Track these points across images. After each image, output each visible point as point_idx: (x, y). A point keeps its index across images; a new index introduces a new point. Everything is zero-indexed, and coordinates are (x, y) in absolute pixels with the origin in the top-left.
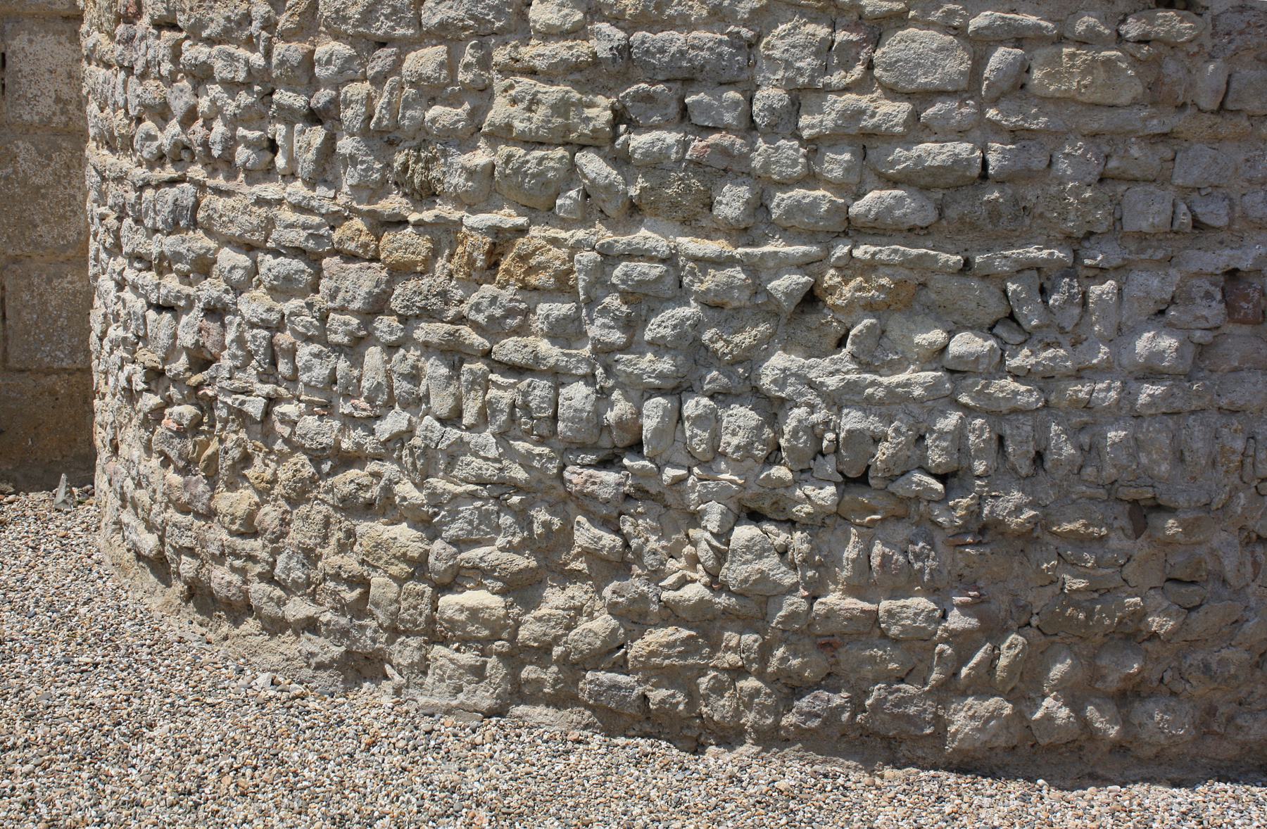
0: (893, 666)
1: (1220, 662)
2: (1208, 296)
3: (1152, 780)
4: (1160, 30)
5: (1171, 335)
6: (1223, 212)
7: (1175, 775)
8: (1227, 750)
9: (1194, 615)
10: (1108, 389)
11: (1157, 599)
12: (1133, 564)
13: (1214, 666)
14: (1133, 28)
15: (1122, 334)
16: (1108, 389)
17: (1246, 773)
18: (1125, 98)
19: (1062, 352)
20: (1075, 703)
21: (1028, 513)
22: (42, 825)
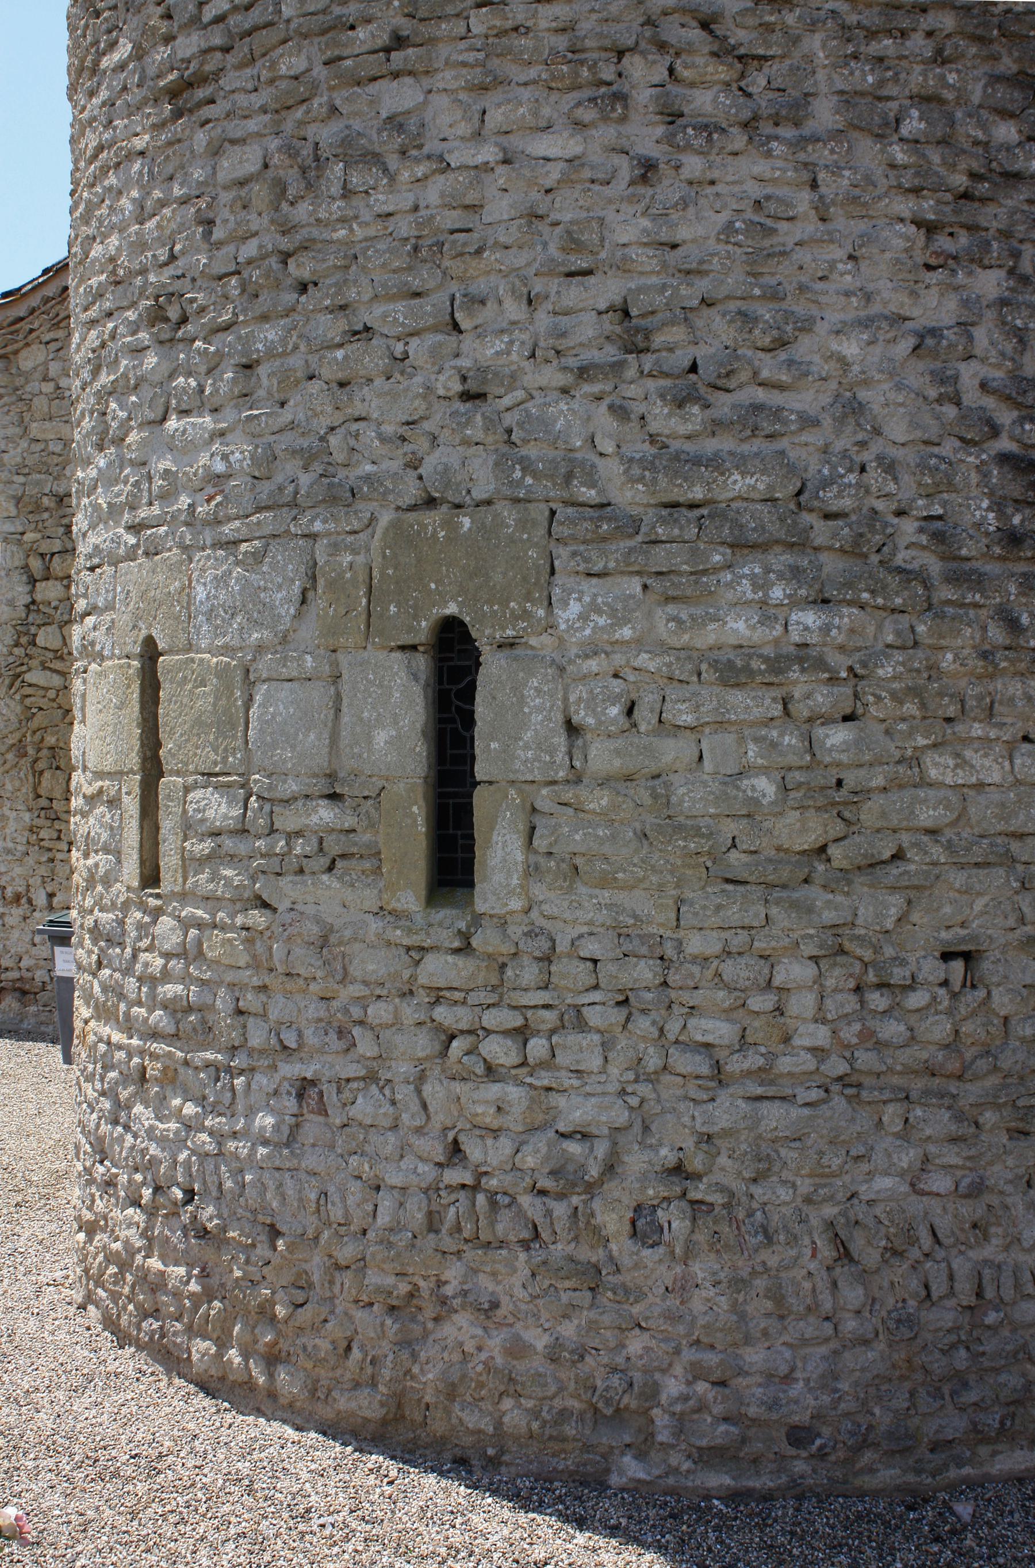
0: (172, 1309)
1: (315, 1346)
2: (289, 1093)
3: (284, 1421)
4: (250, 922)
5: (273, 1116)
6: (294, 1039)
7: (285, 1416)
8: (327, 1412)
9: (300, 1310)
10: (244, 1147)
11: (280, 1295)
12: (270, 1267)
13: (310, 1349)
14: (239, 920)
15: (250, 1113)
16: (244, 1147)
17: (343, 1433)
18: (242, 963)
19: (224, 1120)
20: (246, 1355)
21: (216, 1221)
22: (8, 1415)
